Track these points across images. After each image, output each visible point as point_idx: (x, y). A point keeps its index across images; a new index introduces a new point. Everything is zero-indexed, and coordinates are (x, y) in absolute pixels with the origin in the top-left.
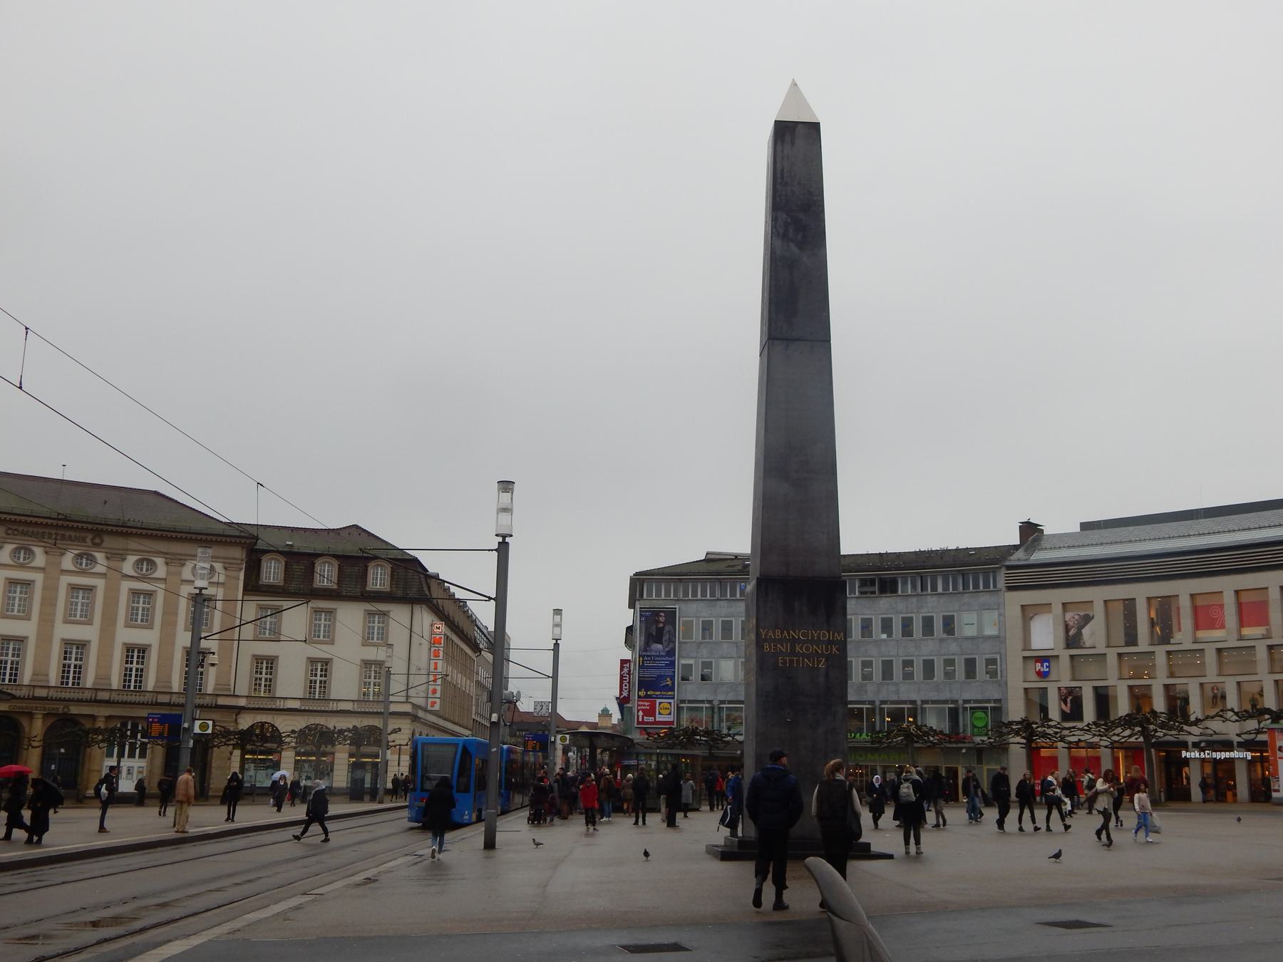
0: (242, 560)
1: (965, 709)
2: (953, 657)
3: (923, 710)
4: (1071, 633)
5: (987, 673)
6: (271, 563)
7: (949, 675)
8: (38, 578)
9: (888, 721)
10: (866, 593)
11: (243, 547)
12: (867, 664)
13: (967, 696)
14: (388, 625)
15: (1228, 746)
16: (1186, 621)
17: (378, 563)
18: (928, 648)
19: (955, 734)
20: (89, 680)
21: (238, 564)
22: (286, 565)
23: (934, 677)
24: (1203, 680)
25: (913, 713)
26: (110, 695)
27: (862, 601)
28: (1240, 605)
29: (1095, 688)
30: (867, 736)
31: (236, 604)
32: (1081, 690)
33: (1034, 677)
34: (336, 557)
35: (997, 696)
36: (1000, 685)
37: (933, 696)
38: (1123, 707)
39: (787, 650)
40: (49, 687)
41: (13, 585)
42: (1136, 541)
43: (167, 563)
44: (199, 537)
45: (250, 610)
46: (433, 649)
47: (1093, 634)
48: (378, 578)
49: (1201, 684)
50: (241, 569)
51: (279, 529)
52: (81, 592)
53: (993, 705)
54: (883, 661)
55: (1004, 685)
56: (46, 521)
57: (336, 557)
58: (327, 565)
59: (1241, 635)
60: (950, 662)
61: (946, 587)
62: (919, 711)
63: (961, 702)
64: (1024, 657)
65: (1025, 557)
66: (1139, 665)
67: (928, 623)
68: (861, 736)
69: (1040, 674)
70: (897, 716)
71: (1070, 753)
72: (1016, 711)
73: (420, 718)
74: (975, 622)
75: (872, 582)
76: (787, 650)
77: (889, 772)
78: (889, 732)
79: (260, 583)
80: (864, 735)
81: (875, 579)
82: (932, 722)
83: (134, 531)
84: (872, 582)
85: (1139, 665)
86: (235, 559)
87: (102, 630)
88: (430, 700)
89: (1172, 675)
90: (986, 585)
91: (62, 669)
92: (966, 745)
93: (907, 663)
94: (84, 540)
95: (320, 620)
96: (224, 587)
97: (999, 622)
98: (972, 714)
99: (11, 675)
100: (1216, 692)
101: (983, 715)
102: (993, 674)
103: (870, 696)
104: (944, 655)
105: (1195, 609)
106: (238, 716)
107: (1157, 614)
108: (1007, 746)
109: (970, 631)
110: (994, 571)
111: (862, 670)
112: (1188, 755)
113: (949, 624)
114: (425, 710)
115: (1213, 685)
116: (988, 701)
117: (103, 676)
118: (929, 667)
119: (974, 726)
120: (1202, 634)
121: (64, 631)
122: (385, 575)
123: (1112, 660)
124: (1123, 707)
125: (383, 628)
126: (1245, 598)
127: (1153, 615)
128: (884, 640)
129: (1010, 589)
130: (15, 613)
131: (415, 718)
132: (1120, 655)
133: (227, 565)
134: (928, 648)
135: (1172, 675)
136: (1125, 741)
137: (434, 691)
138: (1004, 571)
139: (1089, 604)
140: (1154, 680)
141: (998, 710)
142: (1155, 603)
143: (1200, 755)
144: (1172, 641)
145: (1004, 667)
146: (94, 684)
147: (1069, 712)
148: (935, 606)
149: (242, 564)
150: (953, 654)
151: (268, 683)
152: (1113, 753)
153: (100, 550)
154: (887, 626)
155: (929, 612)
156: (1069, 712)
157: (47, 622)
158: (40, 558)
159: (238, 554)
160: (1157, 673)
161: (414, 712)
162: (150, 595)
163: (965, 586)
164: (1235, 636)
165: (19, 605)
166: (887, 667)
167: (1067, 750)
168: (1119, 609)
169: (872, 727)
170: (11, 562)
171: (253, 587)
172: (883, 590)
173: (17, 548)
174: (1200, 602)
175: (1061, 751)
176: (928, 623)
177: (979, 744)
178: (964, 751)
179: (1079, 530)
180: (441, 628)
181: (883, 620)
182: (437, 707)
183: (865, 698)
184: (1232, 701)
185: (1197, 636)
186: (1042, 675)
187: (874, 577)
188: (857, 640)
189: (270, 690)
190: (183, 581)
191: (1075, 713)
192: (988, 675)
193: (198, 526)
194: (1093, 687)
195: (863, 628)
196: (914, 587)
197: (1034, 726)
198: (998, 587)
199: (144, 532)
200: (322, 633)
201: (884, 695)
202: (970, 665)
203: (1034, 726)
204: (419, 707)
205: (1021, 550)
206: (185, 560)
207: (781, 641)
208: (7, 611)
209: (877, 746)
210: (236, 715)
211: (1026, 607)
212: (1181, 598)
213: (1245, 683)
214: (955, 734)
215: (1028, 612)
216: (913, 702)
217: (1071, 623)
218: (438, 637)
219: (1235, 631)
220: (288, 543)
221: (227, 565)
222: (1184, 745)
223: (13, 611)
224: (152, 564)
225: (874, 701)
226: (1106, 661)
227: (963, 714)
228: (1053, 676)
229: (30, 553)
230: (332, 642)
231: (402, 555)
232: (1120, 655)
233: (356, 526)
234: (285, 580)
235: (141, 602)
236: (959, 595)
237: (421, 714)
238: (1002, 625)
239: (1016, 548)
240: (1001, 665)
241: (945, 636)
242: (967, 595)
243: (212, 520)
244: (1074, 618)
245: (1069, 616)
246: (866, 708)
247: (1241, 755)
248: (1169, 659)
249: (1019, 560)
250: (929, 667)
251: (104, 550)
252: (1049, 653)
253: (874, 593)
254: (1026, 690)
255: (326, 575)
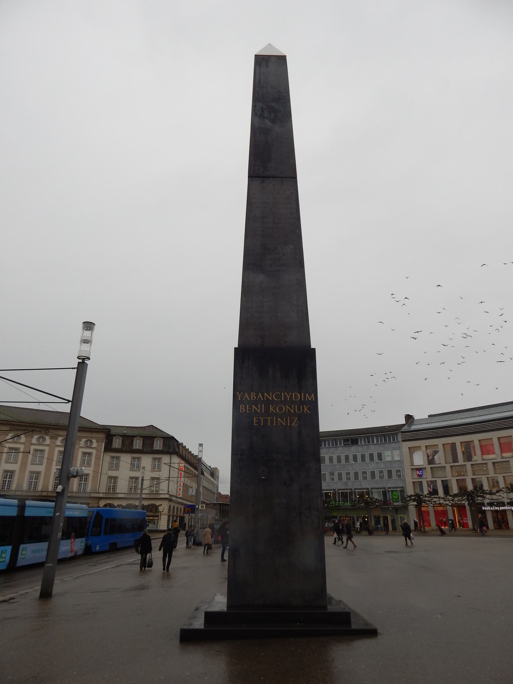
0: (104, 438)
1: (389, 491)
2: (382, 470)
3: (372, 492)
4: (430, 458)
5: (397, 476)
6: (137, 441)
7: (381, 477)
8: (94, 451)
9: (358, 497)
10: (346, 445)
11: (104, 433)
12: (348, 474)
13: (389, 486)
14: (119, 463)
15: (503, 504)
16: (478, 451)
17: (158, 439)
18: (372, 467)
19: (385, 502)
20: (40, 488)
21: (102, 440)
22: (143, 441)
23: (375, 478)
24: (488, 476)
25: (368, 493)
26: (47, 494)
27: (345, 448)
28: (500, 444)
29: (442, 481)
30: (350, 503)
31: (18, 455)
32: (437, 482)
33: (416, 477)
34: (142, 437)
35: (401, 485)
36: (402, 481)
37: (375, 486)
38: (455, 490)
39: (261, 410)
40: (22, 491)
41: (37, 452)
42: (453, 420)
43: (97, 442)
44: (87, 430)
45: (107, 457)
46: (179, 472)
47: (439, 458)
48: (158, 445)
49: (487, 478)
50: (103, 442)
51: (122, 427)
52: (39, 452)
53: (400, 489)
54: (354, 472)
55: (404, 481)
56: (56, 427)
57: (142, 437)
58: (138, 440)
59: (502, 457)
60: (381, 472)
61: (377, 441)
62: (370, 492)
63: (387, 488)
64: (411, 469)
65: (408, 428)
66: (460, 471)
67: (371, 456)
68: (347, 503)
69: (418, 475)
70: (362, 495)
71: (434, 508)
72: (410, 491)
73: (173, 500)
74: (390, 455)
75: (348, 440)
76: (261, 410)
77: (360, 519)
78: (359, 501)
79: (112, 447)
80: (348, 503)
81: (349, 439)
82: (376, 496)
83: (62, 427)
84: (348, 440)
85: (460, 471)
86: (101, 438)
87: (46, 467)
88: (178, 493)
89: (474, 474)
90: (394, 440)
91: (1, 487)
92: (391, 506)
93: (365, 473)
94: (41, 432)
95: (135, 461)
96: (24, 445)
97: (400, 455)
98: (392, 493)
99: (5, 486)
100: (494, 481)
101: (397, 493)
102: (399, 476)
103: (350, 487)
104: (379, 469)
105: (481, 446)
106: (99, 501)
107: (464, 449)
108: (407, 506)
109: (388, 459)
110: (397, 434)
111: (346, 476)
112: (485, 509)
113: (380, 456)
114: (177, 497)
115: (492, 478)
116: (398, 488)
117: (46, 486)
118: (373, 474)
119: (393, 498)
120: (485, 457)
121: (30, 468)
122: (160, 443)
123: (448, 469)
124: (455, 490)
125: (139, 464)
126: (502, 441)
127: (463, 450)
128: (353, 463)
129: (403, 441)
130: (37, 462)
131: (170, 500)
132: (451, 467)
133: (26, 435)
134: (372, 467)
135: (474, 474)
136: (460, 503)
137: (180, 489)
138: (400, 434)
139: (436, 446)
140: (467, 477)
141: (402, 491)
142: (463, 444)
143: (490, 508)
144: (473, 460)
145: (403, 473)
146: (42, 489)
147: (432, 491)
148: (374, 449)
149: (104, 440)
150: (383, 468)
151: (114, 487)
152: (452, 509)
153: (48, 435)
154: (355, 458)
155: (371, 452)
156: (432, 491)
157: (24, 464)
158: (48, 441)
159: (102, 436)
160: (468, 473)
161: (170, 498)
162: (90, 454)
163: (385, 441)
164: (500, 456)
165: (13, 458)
166: (356, 474)
167: (433, 507)
168: (449, 448)
169: (351, 499)
170: (36, 443)
171: (108, 449)
172: (353, 443)
173: (86, 441)
174: (483, 443)
175: (431, 509)
176: (371, 456)
177: (397, 506)
178: (390, 509)
179: (428, 417)
180: (183, 464)
181: (329, 457)
182: (181, 496)
183: (348, 488)
184: (502, 485)
185: (483, 457)
186: (420, 476)
187: (348, 438)
188: (343, 464)
189: (114, 490)
190: (56, 445)
191: (435, 492)
192: (397, 477)
193: (88, 425)
194: (441, 480)
195: (362, 458)
196: (365, 442)
197: (421, 497)
198: (398, 440)
199: (85, 429)
200: (156, 467)
201: (355, 486)
202: (390, 472)
203: (421, 497)
204: (174, 496)
205: (406, 425)
206: (81, 439)
207: (256, 403)
208: (8, 460)
209: (354, 508)
210: (98, 501)
211: (481, 441)
212: (475, 442)
213: (506, 477)
214: (385, 502)
215: (412, 450)
216: (368, 489)
217: (429, 454)
218: (181, 467)
219: (500, 455)
220: (124, 432)
221: (98, 440)
222: (483, 505)
223: (10, 460)
224: (91, 442)
225: (352, 489)
226: (446, 469)
227: (388, 493)
228: (424, 476)
229: (44, 439)
230: (118, 470)
231: (168, 436)
232: (451, 467)
233: (152, 426)
234: (143, 447)
235: (87, 457)
236: (383, 444)
237: (174, 498)
238: (401, 455)
239: (404, 425)
240: (402, 472)
241: (379, 461)
242: (386, 444)
243: (93, 423)
244: (430, 452)
245: (428, 451)
246: (349, 492)
247: (509, 508)
248: (472, 468)
249: (406, 429)
250: (373, 474)
251: (49, 435)
252: (422, 467)
253: (349, 444)
254: (413, 482)
255: (138, 444)
